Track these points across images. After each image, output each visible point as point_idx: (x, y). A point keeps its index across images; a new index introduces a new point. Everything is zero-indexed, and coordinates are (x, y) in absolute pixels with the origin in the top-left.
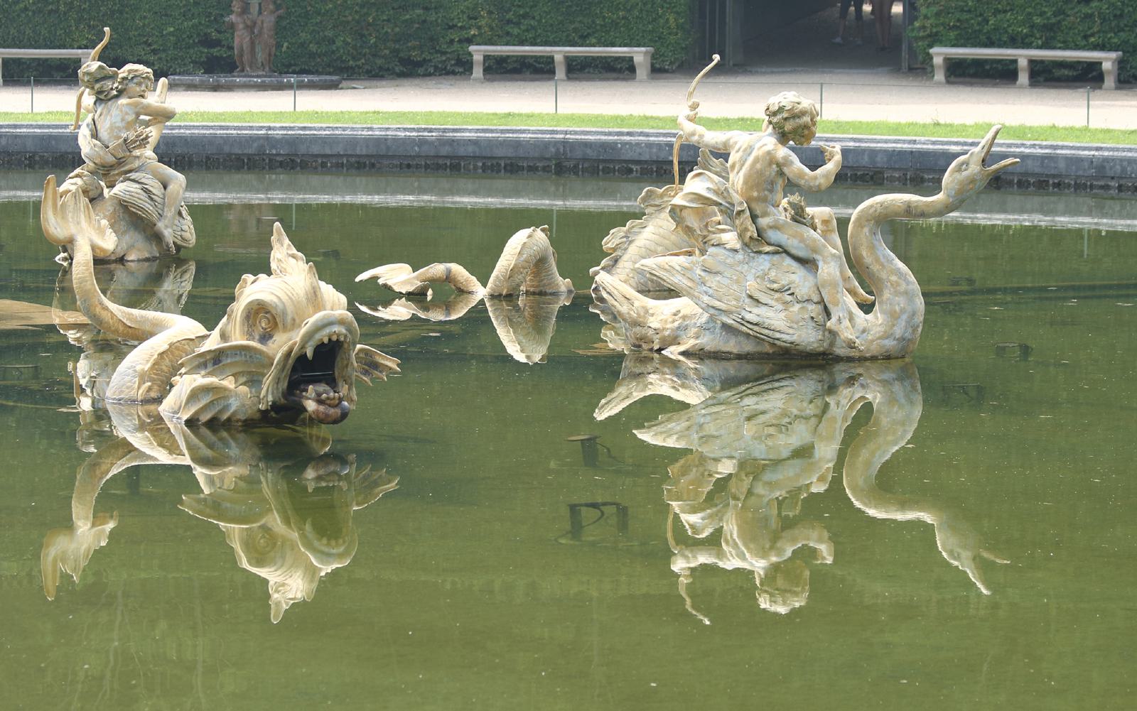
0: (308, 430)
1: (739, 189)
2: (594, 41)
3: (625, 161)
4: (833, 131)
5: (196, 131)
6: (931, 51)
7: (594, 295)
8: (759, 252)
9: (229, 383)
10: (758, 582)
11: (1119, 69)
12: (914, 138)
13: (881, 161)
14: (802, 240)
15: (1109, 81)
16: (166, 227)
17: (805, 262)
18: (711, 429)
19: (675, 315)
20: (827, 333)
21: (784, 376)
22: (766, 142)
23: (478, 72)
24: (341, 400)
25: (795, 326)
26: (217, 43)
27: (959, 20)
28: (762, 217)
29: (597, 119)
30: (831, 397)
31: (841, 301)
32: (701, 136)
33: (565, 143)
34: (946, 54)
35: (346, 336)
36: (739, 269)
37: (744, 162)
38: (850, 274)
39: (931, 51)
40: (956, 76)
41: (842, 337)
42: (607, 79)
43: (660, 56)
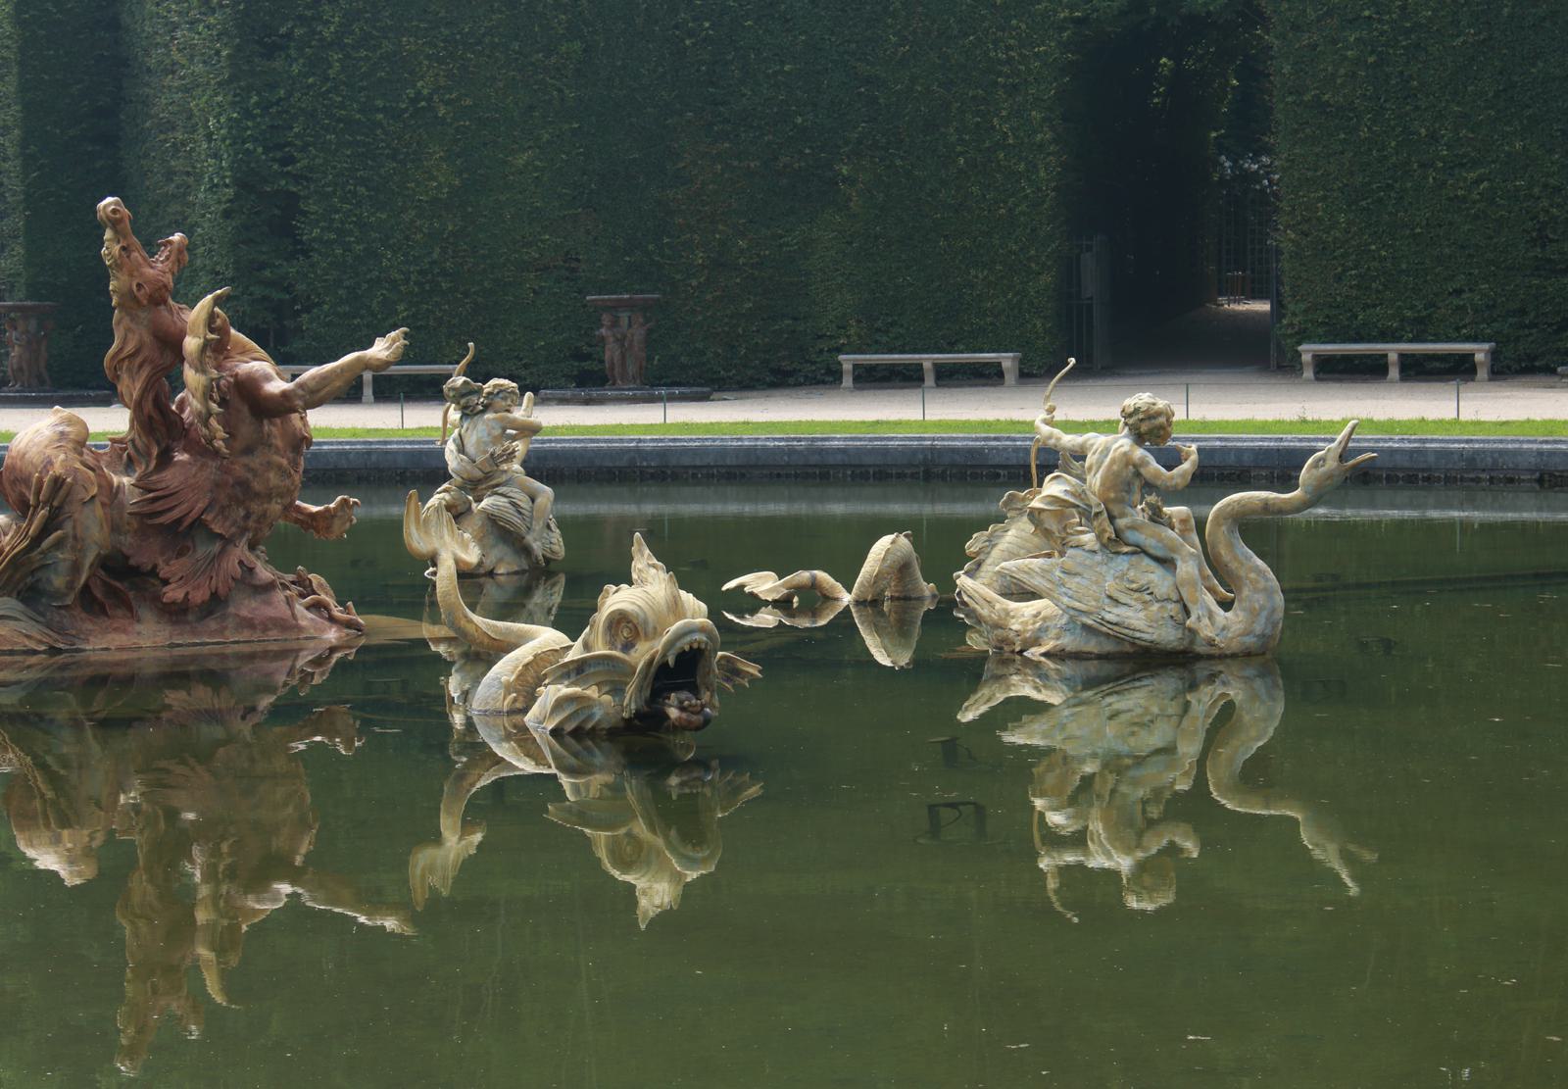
0: (671, 737)
2: (962, 347)
3: (992, 466)
4: (1199, 432)
5: (567, 445)
6: (1300, 348)
8: (1118, 553)
9: (592, 692)
10: (1125, 881)
11: (1492, 360)
13: (1247, 459)
14: (1160, 540)
15: (1482, 373)
16: (535, 540)
17: (1166, 562)
18: (1073, 729)
19: (1036, 616)
20: (1186, 632)
22: (1122, 443)
23: (848, 381)
24: (703, 706)
26: (588, 357)
27: (1328, 316)
28: (1120, 517)
30: (1192, 694)
32: (1058, 439)
33: (932, 449)
35: (707, 644)
42: (976, 385)
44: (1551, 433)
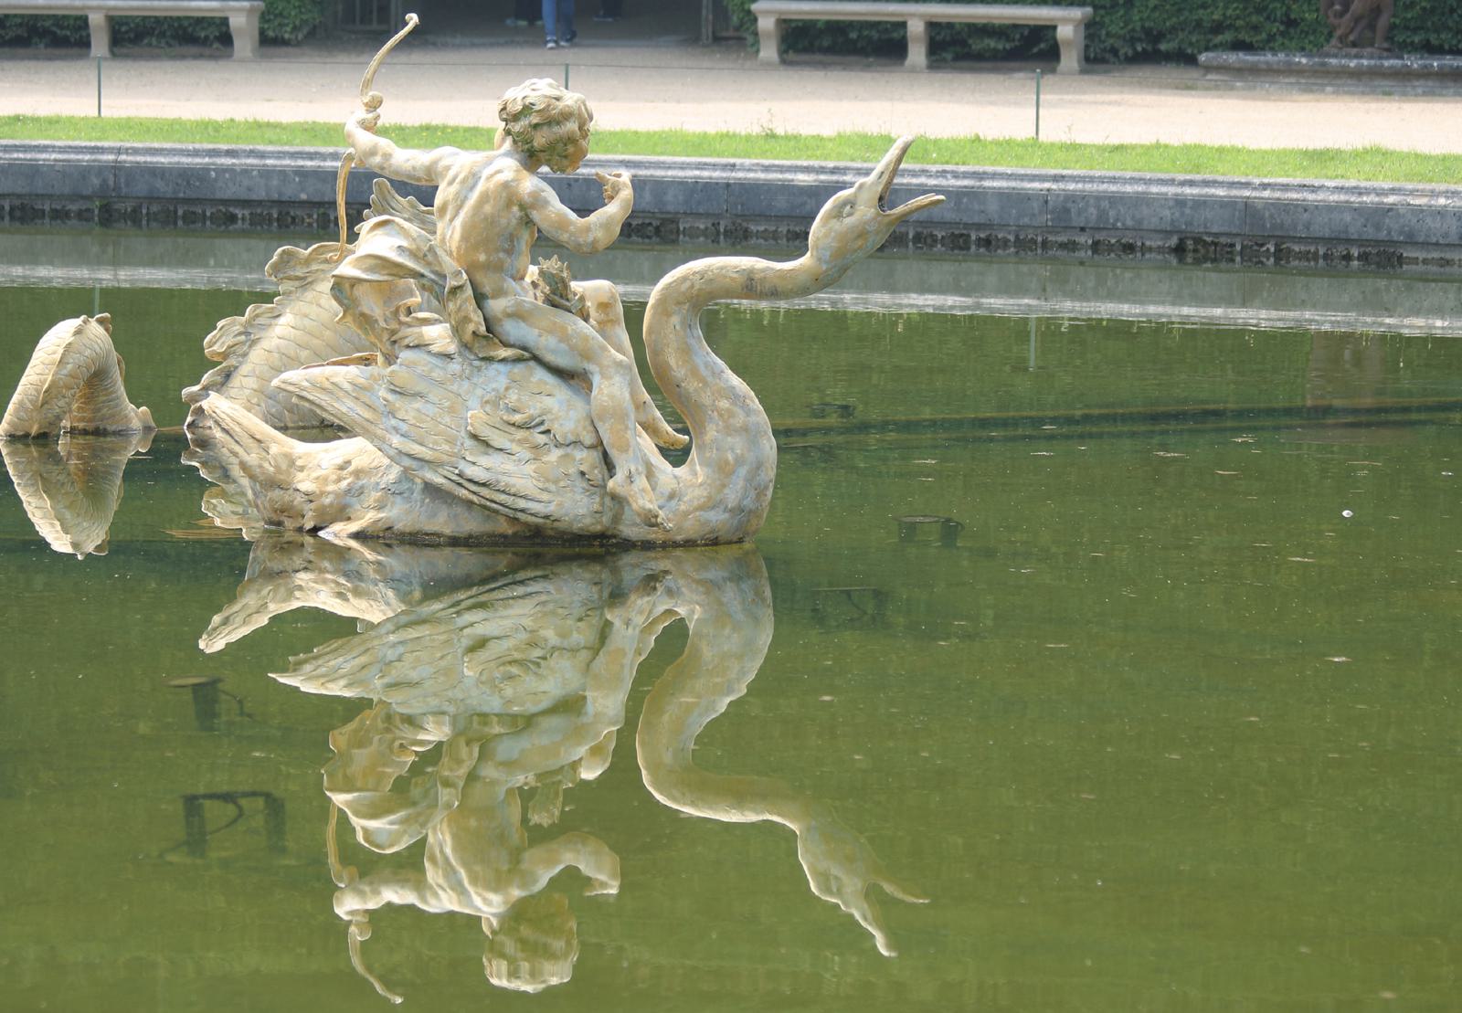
1: (454, 249)
3: (225, 202)
6: (754, 7)
7: (189, 436)
8: (489, 359)
12: (732, 161)
14: (565, 338)
15: (1070, 59)
17: (573, 377)
19: (341, 468)
20: (607, 500)
21: (533, 575)
22: (503, 166)
25: (553, 487)
28: (494, 297)
29: (172, 127)
30: (617, 611)
31: (632, 442)
32: (387, 156)
33: (117, 168)
34: (781, 13)
36: (455, 387)
37: (463, 202)
38: (647, 397)
39: (754, 7)
40: (797, 51)
41: (634, 506)
42: (183, 57)
43: (276, 16)
44: (1197, 168)
